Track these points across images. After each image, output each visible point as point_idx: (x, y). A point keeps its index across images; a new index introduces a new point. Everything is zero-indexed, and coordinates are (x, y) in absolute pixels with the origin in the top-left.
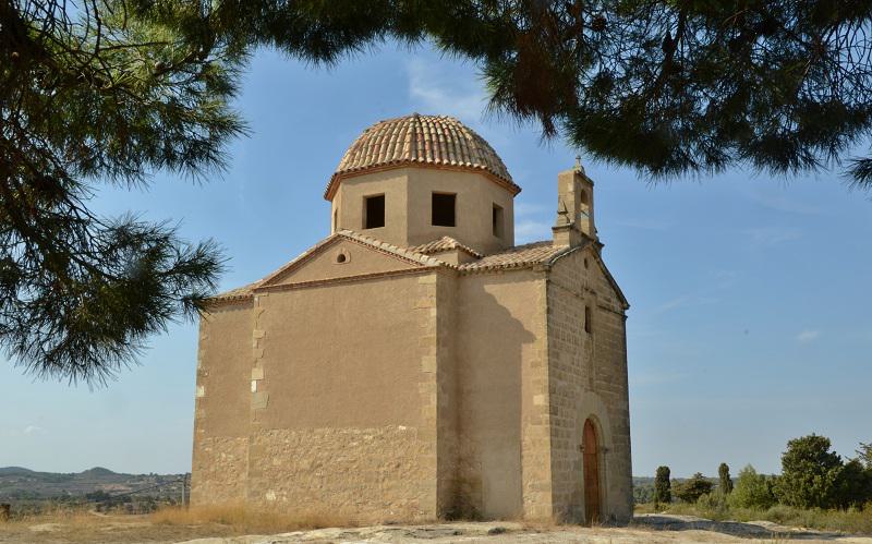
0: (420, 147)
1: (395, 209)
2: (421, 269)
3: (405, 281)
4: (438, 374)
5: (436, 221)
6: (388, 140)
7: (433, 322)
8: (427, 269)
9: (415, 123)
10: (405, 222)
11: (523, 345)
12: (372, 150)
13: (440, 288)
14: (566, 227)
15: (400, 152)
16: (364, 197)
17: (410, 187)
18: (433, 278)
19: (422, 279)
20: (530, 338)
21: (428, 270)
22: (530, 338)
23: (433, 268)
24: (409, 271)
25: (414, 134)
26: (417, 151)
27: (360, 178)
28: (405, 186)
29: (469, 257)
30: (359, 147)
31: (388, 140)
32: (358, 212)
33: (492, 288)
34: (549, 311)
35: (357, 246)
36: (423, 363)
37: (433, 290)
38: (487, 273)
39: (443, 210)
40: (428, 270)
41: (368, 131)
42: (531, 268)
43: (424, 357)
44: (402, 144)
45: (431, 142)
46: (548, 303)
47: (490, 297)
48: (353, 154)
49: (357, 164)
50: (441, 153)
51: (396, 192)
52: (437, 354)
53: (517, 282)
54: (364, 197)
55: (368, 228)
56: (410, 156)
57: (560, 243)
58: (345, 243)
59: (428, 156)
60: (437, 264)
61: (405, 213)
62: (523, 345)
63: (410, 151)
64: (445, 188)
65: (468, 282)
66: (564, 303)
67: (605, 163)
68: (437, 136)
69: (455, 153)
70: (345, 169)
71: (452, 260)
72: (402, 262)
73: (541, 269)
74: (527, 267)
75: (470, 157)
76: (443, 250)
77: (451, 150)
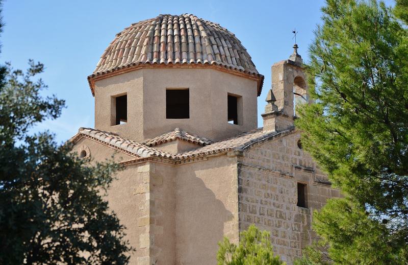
0: (155, 49)
1: (134, 107)
2: (139, 160)
3: (129, 171)
4: (151, 250)
5: (170, 115)
6: (130, 44)
7: (148, 204)
8: (143, 160)
9: (155, 25)
10: (142, 118)
11: (225, 223)
12: (118, 54)
13: (153, 176)
14: (272, 114)
15: (139, 55)
16: (112, 97)
17: (145, 87)
18: (146, 168)
19: (140, 169)
20: (231, 217)
21: (144, 161)
22: (231, 217)
23: (147, 159)
24: (131, 162)
25: (152, 38)
26: (152, 53)
27: (108, 80)
28: (142, 86)
29: (192, 146)
30: (109, 51)
31: (130, 44)
32: (108, 110)
33: (200, 173)
34: (240, 190)
35: (94, 142)
36: (141, 240)
37: (147, 178)
38: (200, 160)
39: (178, 104)
40: (144, 161)
41: (119, 35)
42: (226, 154)
43: (142, 235)
44: (141, 47)
45: (166, 44)
46: (239, 183)
47: (200, 182)
48: (105, 58)
49: (108, 67)
50: (174, 53)
51: (133, 87)
52: (150, 232)
53: (218, 167)
54: (112, 97)
55: (126, 119)
56: (146, 58)
57: (268, 128)
58: (87, 140)
59: (161, 57)
60: (149, 156)
61: (142, 110)
62: (225, 223)
63: (146, 53)
64: (178, 84)
65: (183, 168)
66: (264, 182)
67: (31, 127)
68: (173, 36)
69: (188, 52)
70: (96, 73)
71: (171, 151)
72: (125, 155)
73: (233, 154)
74: (223, 153)
75: (202, 53)
76: (166, 141)
77: (184, 49)
